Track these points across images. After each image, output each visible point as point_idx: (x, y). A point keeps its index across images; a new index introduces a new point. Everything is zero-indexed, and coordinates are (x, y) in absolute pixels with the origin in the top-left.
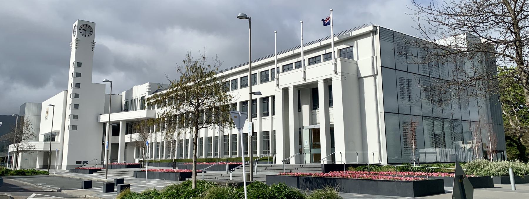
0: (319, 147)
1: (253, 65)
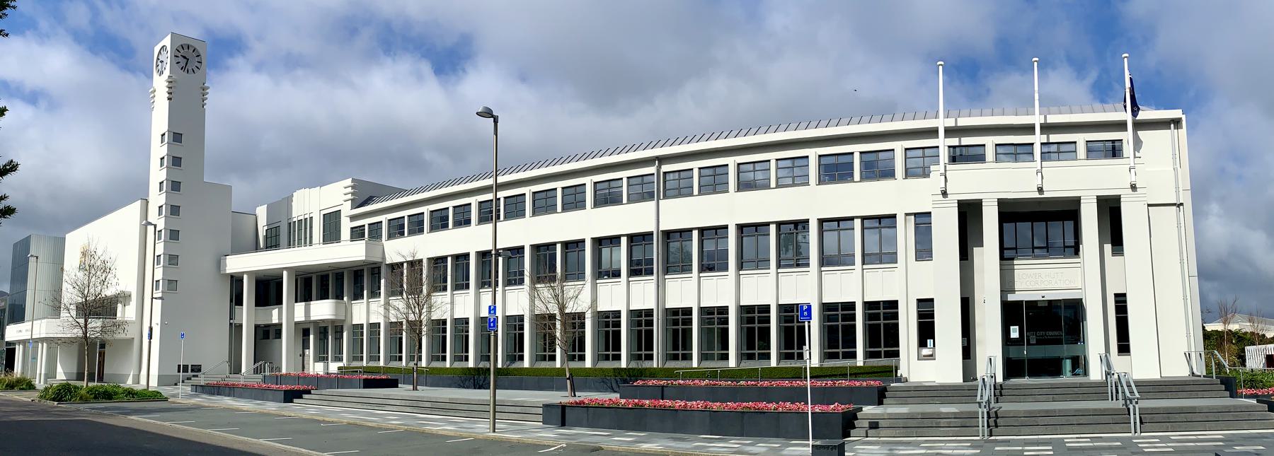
1: (501, 179)
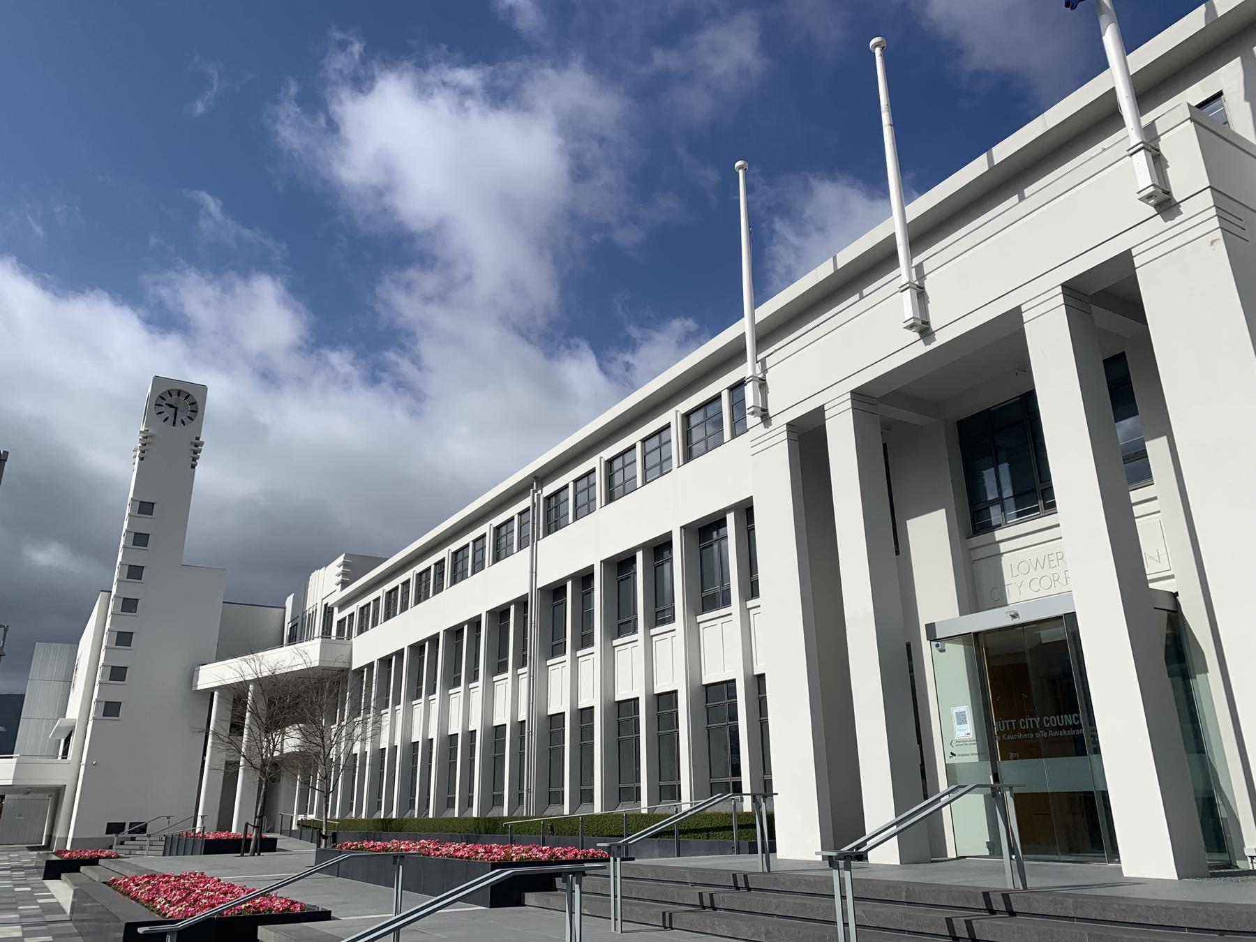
0: (1082, 742)
